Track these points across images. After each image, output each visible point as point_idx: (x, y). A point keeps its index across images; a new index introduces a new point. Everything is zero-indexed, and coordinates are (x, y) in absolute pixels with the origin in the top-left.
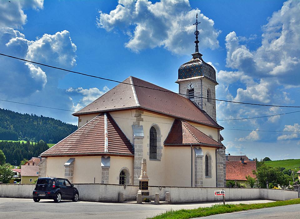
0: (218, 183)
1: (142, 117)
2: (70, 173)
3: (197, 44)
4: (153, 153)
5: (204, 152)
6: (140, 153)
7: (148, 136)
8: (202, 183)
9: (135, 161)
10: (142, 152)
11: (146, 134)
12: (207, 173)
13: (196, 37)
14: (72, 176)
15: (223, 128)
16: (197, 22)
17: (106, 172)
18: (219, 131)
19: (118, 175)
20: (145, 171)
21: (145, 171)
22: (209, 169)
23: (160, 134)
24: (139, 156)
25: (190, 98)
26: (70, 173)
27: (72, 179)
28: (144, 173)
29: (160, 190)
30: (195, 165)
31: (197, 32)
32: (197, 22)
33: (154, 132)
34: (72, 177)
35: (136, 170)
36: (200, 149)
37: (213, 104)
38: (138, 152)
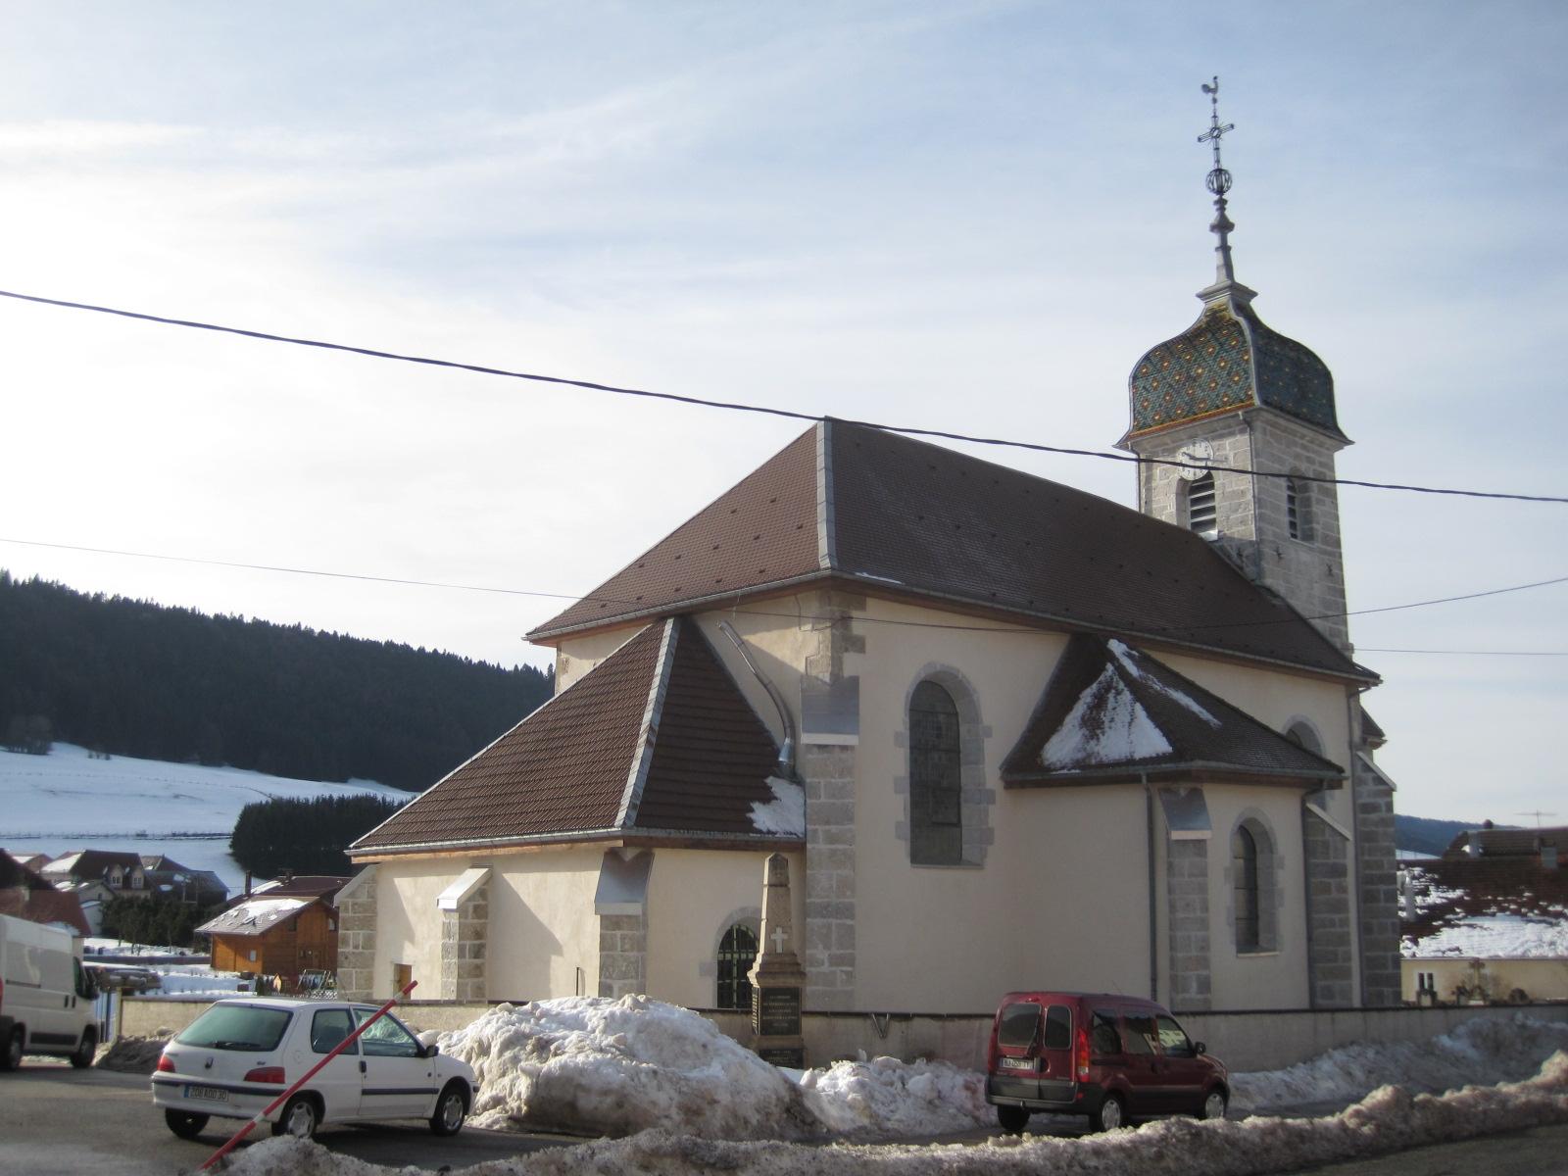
0: (1321, 983)
1: (857, 628)
2: (468, 943)
3: (1224, 240)
4: (937, 820)
5: (1224, 810)
6: (834, 828)
7: (897, 735)
8: (1205, 985)
9: (808, 872)
10: (851, 820)
11: (886, 716)
12: (1251, 934)
13: (1216, 202)
14: (477, 961)
15: (535, 642)
16: (1216, 122)
17: (623, 938)
18: (1353, 695)
19: (706, 949)
20: (779, 930)
21: (779, 930)
22: (1262, 904)
23: (976, 719)
24: (832, 843)
25: (1195, 525)
26: (468, 943)
27: (477, 976)
28: (773, 937)
29: (884, 1034)
30: (1169, 884)
31: (1219, 172)
32: (1216, 122)
33: (936, 712)
34: (478, 967)
35: (819, 921)
36: (1196, 795)
37: (1325, 552)
38: (828, 823)
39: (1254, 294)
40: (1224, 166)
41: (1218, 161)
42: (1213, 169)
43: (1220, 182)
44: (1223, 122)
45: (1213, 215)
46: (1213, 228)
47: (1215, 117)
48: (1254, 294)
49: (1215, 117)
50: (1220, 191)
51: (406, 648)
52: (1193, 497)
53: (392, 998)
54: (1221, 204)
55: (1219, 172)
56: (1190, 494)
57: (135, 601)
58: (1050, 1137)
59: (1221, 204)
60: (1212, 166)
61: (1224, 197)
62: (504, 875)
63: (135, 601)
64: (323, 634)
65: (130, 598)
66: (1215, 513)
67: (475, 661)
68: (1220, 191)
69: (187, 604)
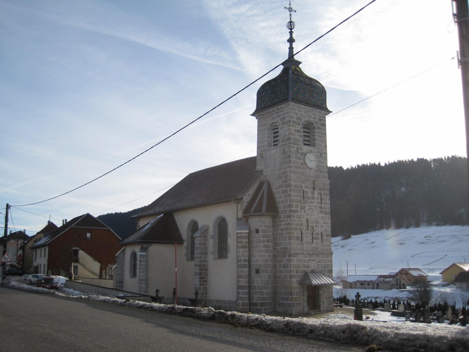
31: (291, 22)
39: (301, 63)
40: (292, 20)
41: (291, 19)
42: (289, 21)
43: (291, 25)
44: (288, 6)
45: (288, 37)
46: (288, 41)
47: (290, 4)
48: (301, 63)
49: (290, 4)
50: (291, 29)
51: (112, 214)
52: (274, 131)
53: (4, 261)
54: (291, 33)
55: (291, 22)
56: (273, 130)
57: (335, 167)
58: (244, 313)
59: (291, 33)
60: (289, 20)
61: (290, 31)
62: (8, 235)
63: (335, 167)
64: (117, 213)
65: (435, 158)
66: (278, 133)
67: (114, 213)
68: (291, 29)
69: (367, 160)
